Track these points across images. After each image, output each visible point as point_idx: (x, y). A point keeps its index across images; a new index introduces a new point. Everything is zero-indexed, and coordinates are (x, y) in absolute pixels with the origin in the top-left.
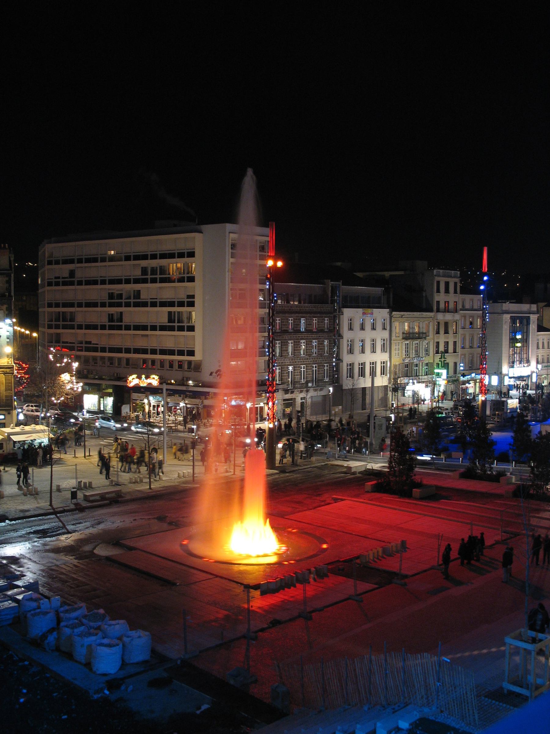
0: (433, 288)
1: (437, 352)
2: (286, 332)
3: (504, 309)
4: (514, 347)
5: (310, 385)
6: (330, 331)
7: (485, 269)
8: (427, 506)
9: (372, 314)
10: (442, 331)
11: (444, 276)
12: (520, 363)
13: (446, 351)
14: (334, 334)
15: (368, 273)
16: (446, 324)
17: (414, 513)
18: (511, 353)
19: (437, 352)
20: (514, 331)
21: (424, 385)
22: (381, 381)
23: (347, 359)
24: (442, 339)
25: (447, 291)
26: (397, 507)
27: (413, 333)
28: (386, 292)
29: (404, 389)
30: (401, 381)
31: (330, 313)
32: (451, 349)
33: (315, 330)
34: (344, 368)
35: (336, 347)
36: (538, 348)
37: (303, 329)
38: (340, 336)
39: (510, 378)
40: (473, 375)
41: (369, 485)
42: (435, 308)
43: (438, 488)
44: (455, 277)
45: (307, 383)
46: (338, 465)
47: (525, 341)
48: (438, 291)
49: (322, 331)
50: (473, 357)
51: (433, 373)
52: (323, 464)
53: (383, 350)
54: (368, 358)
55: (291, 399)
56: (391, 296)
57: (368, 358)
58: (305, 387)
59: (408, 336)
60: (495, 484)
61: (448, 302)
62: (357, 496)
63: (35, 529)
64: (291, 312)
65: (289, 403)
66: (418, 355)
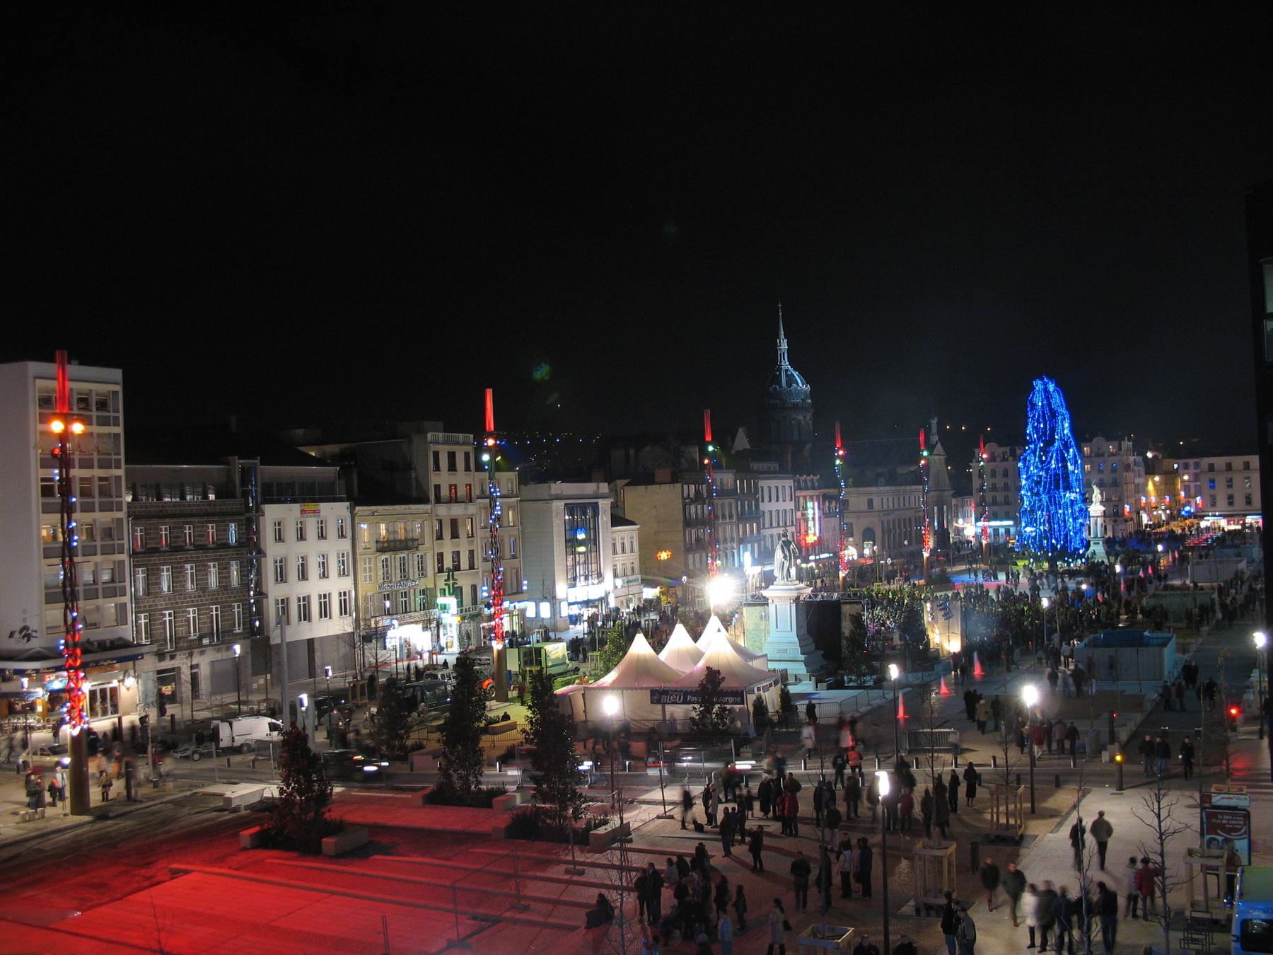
1: (441, 570)
2: (155, 551)
3: (553, 492)
4: (574, 553)
6: (240, 544)
8: (343, 872)
9: (316, 512)
11: (446, 443)
12: (586, 578)
13: (457, 568)
14: (250, 548)
15: (345, 445)
16: (454, 523)
17: (313, 890)
18: (570, 563)
19: (441, 570)
20: (573, 528)
21: (420, 626)
22: (338, 625)
23: (275, 592)
24: (447, 547)
25: (452, 467)
26: (284, 881)
27: (395, 541)
28: (345, 472)
29: (383, 636)
30: (376, 623)
31: (240, 514)
32: (464, 563)
33: (211, 545)
36: (615, 552)
37: (232, 539)
38: (261, 553)
39: (570, 604)
41: (246, 835)
42: (432, 497)
43: (374, 828)
44: (464, 444)
45: (200, 638)
46: (214, 794)
47: (593, 542)
48: (437, 468)
51: (434, 606)
52: (188, 793)
54: (314, 588)
55: (173, 670)
56: (355, 477)
57: (314, 588)
58: (194, 646)
59: (386, 546)
60: (482, 812)
62: (220, 861)
63: (139, 806)
64: (163, 515)
65: (164, 677)
66: (405, 577)
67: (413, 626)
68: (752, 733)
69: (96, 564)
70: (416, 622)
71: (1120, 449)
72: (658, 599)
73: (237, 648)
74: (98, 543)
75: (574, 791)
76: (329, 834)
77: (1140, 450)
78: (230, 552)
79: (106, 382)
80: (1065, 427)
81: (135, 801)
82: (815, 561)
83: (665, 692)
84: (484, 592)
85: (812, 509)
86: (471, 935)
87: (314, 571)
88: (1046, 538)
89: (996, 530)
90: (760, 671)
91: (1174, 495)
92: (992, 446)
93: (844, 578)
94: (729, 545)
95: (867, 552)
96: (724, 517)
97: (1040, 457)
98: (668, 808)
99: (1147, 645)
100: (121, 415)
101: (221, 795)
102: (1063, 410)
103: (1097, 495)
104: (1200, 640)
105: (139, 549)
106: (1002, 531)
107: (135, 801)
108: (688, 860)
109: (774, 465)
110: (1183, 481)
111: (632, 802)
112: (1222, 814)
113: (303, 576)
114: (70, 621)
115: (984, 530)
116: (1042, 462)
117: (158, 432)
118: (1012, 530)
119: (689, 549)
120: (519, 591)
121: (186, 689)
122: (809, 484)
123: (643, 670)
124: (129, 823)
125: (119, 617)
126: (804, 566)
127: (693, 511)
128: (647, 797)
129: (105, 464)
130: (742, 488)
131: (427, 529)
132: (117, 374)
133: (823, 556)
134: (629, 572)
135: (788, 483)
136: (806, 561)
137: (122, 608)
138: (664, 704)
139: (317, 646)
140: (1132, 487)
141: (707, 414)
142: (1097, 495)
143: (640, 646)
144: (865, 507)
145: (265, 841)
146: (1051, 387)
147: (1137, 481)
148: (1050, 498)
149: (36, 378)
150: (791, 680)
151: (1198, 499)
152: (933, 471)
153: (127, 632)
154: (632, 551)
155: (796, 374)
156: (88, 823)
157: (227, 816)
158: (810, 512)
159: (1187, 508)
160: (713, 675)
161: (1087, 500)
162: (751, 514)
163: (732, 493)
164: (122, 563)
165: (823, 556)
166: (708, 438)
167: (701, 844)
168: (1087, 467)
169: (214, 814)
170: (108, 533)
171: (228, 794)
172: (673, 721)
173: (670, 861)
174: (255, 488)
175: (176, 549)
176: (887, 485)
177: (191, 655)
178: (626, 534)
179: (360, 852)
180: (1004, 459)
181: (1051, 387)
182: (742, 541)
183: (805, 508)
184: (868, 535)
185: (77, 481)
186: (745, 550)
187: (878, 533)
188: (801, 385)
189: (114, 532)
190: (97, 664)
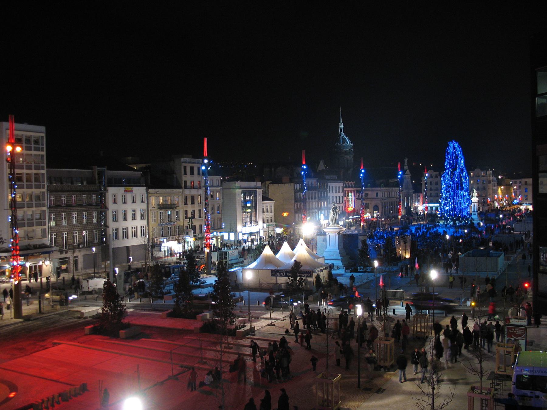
0: (181, 173)
1: (186, 218)
4: (246, 212)
5: (81, 246)
6: (97, 205)
7: (206, 153)
9: (132, 191)
10: (189, 202)
12: (251, 223)
13: (193, 217)
14: (102, 208)
16: (193, 198)
19: (186, 218)
22: (139, 241)
23: (112, 225)
25: (192, 173)
27: (166, 205)
28: (144, 174)
29: (160, 246)
31: (98, 191)
32: (197, 215)
34: (110, 231)
35: (103, 218)
36: (263, 212)
38: (106, 208)
39: (243, 234)
40: (215, 233)
41: (87, 328)
42: (183, 186)
45: (79, 245)
46: (77, 311)
47: (254, 207)
48: (185, 173)
49: (91, 205)
50: (214, 220)
52: (66, 310)
53: (142, 218)
54: (130, 224)
56: (149, 177)
57: (130, 224)
59: (163, 207)
60: (192, 321)
61: (193, 181)
63: (44, 315)
64: (63, 191)
65: (63, 261)
67: (174, 242)
68: (314, 290)
69: (33, 211)
70: (175, 240)
71: (487, 174)
72: (282, 233)
73: (94, 249)
74: (34, 202)
75: (231, 313)
76: (122, 329)
77: (495, 175)
78: (93, 207)
79: (38, 132)
80: (462, 163)
81: (43, 313)
82: (352, 219)
83: (277, 271)
84: (205, 228)
85: (351, 196)
86: (180, 374)
87: (130, 216)
88: (452, 211)
89: (432, 208)
90: (319, 263)
91: (510, 195)
92: (431, 171)
93: (363, 226)
94: (314, 211)
95: (375, 215)
96: (312, 198)
97: (451, 176)
98: (273, 321)
99: (492, 256)
100: (45, 147)
101: (80, 311)
102: (461, 156)
103: (475, 193)
104: (515, 255)
105: (52, 205)
106: (434, 208)
107: (43, 313)
108: (278, 343)
109: (335, 177)
110: (514, 189)
111: (258, 318)
112: (514, 328)
113: (125, 219)
114: (14, 234)
115: (427, 208)
116: (451, 178)
117: (60, 155)
118: (439, 208)
119: (296, 212)
120: (221, 228)
121: (72, 267)
122: (350, 185)
123: (268, 261)
124: (39, 322)
125: (42, 234)
126: (347, 220)
127: (298, 195)
128: (265, 316)
129: (37, 168)
130: (320, 186)
131: (180, 200)
132: (43, 129)
133: (355, 217)
134: (269, 221)
135: (341, 185)
136: (349, 219)
137: (44, 231)
138: (277, 276)
139: (131, 249)
140: (491, 191)
141: (304, 152)
142: (475, 193)
143: (267, 251)
144: (374, 196)
145: (96, 331)
146: (456, 145)
147: (494, 188)
148: (454, 193)
149: (6, 129)
150: (335, 268)
151: (520, 196)
152: (405, 181)
153: (46, 241)
154: (271, 212)
155: (347, 138)
156: (21, 322)
157: (81, 320)
158: (350, 197)
159: (515, 201)
160: (297, 264)
161: (470, 194)
162: (323, 197)
163: (316, 188)
164: (44, 211)
165: (355, 217)
166: (304, 163)
167: (284, 337)
168: (472, 181)
169: (76, 319)
170: (38, 198)
171: (84, 311)
172: (280, 285)
173: (270, 344)
174: (105, 179)
175: (69, 205)
176: (385, 186)
177: (74, 252)
178: (268, 204)
179: (135, 337)
180: (436, 177)
181: (456, 145)
182: (320, 209)
183: (348, 196)
184: (376, 208)
185: (25, 175)
186: (321, 213)
187: (380, 207)
188: (349, 143)
189: (41, 198)
190: (32, 255)
